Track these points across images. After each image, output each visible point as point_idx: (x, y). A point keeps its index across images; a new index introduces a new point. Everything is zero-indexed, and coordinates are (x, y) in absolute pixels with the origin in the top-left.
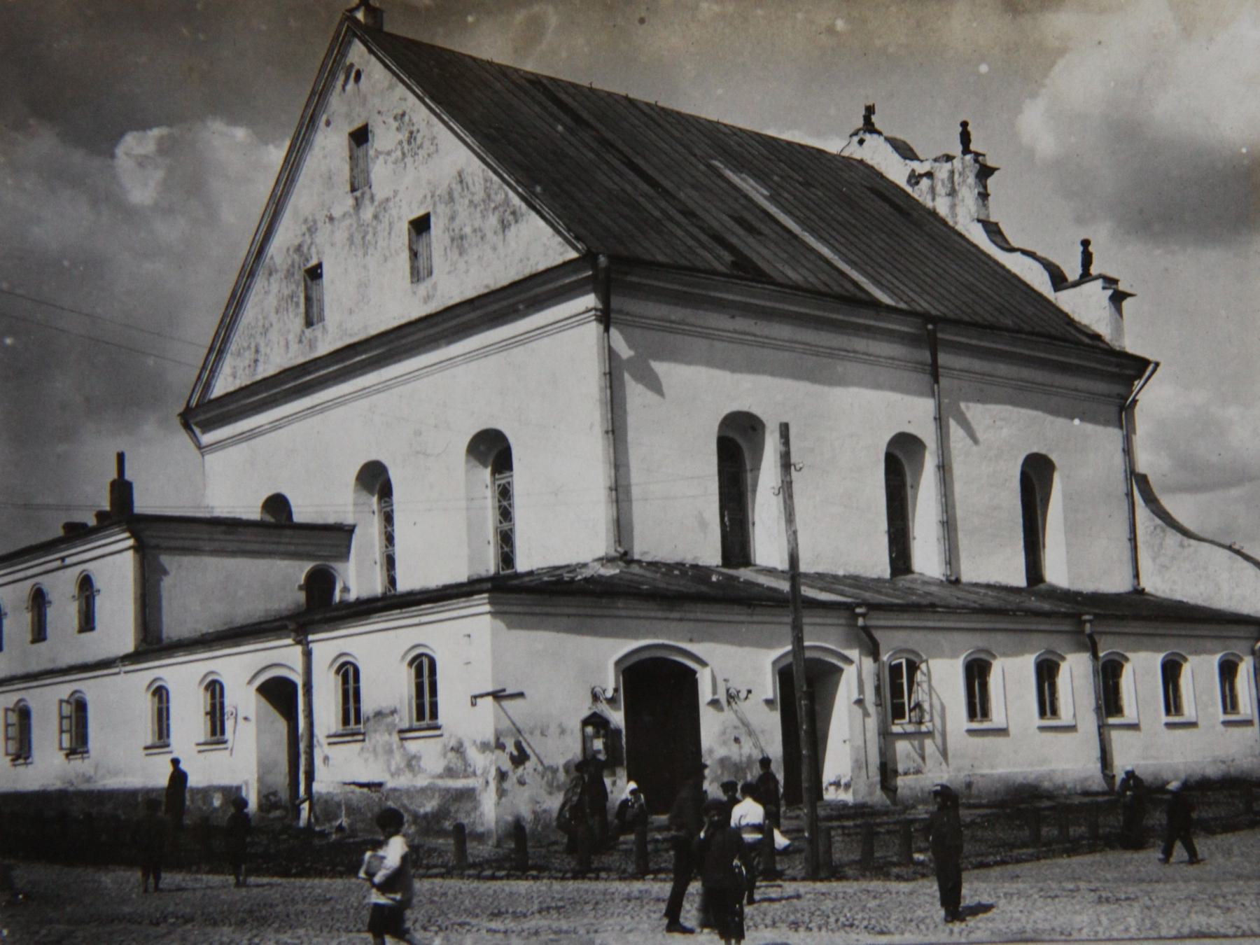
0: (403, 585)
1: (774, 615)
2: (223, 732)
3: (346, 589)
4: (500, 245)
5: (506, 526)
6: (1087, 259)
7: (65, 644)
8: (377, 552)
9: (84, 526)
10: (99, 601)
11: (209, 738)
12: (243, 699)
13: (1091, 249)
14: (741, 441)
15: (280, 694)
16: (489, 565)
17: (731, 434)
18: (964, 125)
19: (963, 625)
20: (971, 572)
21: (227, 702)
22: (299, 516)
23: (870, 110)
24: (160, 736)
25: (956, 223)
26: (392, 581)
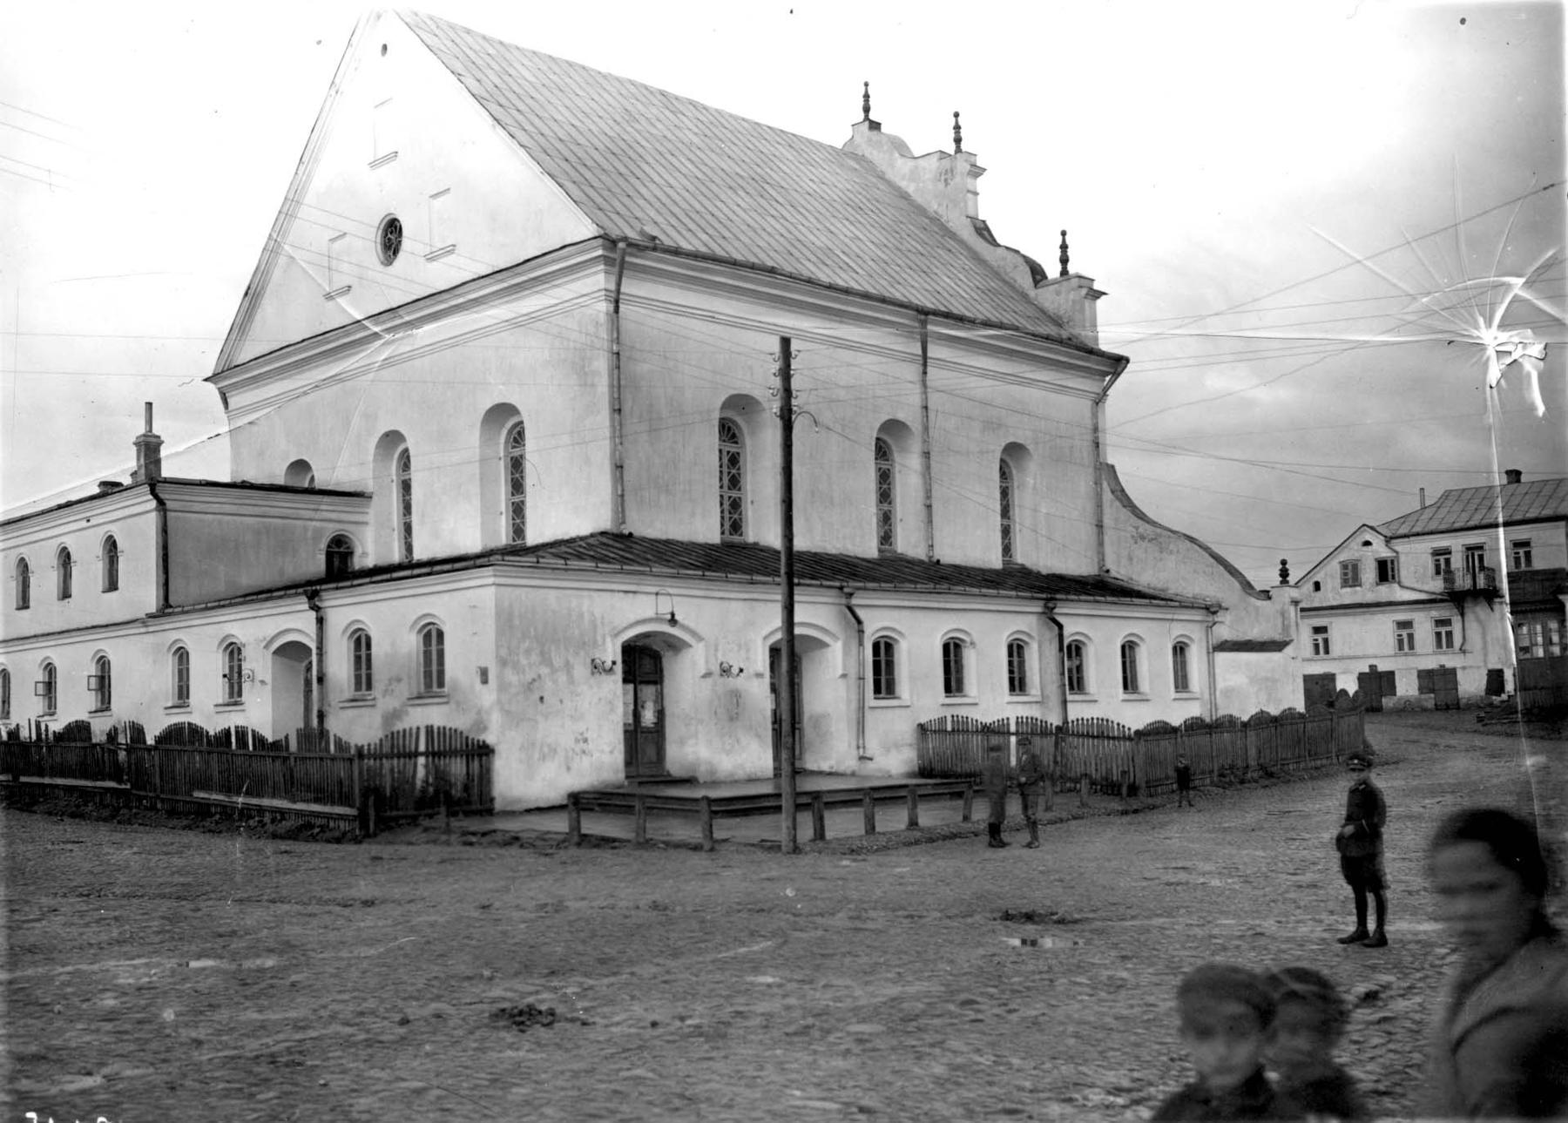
0: (419, 554)
2: (240, 695)
3: (365, 554)
5: (517, 499)
7: (89, 600)
8: (396, 519)
9: (118, 484)
11: (227, 700)
12: (258, 663)
14: (739, 420)
15: (643, 662)
16: (503, 538)
17: (729, 414)
19: (906, 603)
21: (245, 666)
24: (180, 697)
26: (409, 548)
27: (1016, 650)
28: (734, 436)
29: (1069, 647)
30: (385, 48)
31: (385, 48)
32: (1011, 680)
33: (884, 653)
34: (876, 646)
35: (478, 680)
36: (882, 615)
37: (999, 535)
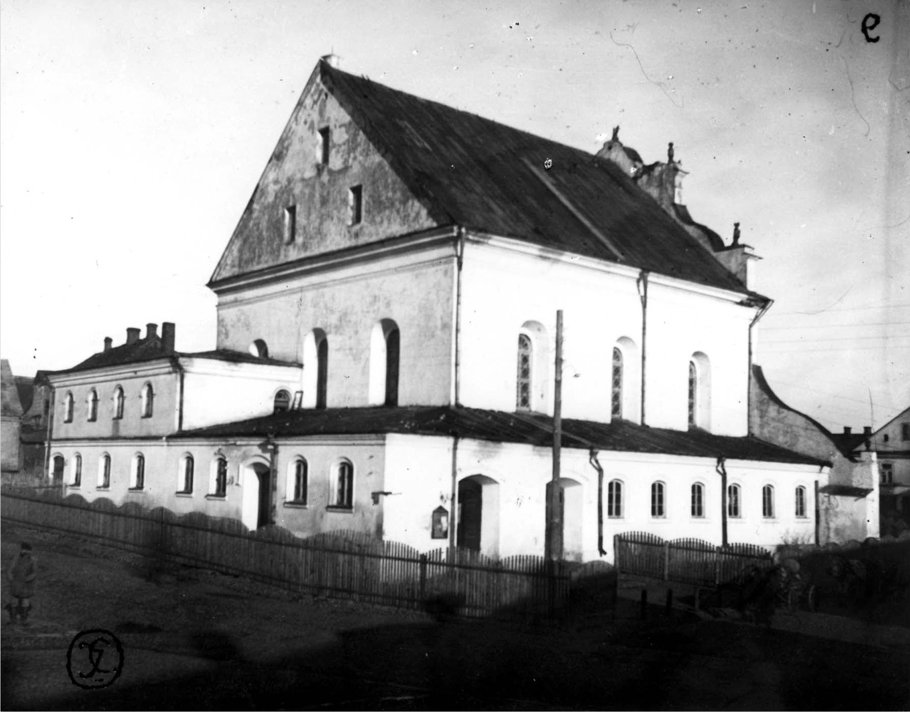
1: (607, 266)
4: (402, 209)
6: (737, 235)
10: (155, 399)
13: (740, 228)
18: (671, 145)
20: (584, 454)
22: (270, 355)
23: (616, 131)
25: (662, 204)
27: (697, 491)
28: (526, 345)
29: (730, 488)
30: (576, 376)
31: (576, 376)
32: (693, 508)
33: (616, 489)
34: (611, 485)
35: (372, 501)
36: (617, 463)
37: (687, 409)
